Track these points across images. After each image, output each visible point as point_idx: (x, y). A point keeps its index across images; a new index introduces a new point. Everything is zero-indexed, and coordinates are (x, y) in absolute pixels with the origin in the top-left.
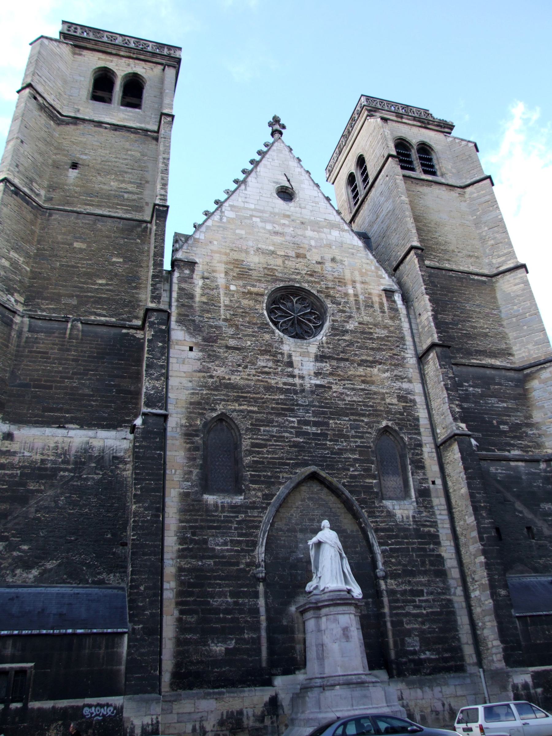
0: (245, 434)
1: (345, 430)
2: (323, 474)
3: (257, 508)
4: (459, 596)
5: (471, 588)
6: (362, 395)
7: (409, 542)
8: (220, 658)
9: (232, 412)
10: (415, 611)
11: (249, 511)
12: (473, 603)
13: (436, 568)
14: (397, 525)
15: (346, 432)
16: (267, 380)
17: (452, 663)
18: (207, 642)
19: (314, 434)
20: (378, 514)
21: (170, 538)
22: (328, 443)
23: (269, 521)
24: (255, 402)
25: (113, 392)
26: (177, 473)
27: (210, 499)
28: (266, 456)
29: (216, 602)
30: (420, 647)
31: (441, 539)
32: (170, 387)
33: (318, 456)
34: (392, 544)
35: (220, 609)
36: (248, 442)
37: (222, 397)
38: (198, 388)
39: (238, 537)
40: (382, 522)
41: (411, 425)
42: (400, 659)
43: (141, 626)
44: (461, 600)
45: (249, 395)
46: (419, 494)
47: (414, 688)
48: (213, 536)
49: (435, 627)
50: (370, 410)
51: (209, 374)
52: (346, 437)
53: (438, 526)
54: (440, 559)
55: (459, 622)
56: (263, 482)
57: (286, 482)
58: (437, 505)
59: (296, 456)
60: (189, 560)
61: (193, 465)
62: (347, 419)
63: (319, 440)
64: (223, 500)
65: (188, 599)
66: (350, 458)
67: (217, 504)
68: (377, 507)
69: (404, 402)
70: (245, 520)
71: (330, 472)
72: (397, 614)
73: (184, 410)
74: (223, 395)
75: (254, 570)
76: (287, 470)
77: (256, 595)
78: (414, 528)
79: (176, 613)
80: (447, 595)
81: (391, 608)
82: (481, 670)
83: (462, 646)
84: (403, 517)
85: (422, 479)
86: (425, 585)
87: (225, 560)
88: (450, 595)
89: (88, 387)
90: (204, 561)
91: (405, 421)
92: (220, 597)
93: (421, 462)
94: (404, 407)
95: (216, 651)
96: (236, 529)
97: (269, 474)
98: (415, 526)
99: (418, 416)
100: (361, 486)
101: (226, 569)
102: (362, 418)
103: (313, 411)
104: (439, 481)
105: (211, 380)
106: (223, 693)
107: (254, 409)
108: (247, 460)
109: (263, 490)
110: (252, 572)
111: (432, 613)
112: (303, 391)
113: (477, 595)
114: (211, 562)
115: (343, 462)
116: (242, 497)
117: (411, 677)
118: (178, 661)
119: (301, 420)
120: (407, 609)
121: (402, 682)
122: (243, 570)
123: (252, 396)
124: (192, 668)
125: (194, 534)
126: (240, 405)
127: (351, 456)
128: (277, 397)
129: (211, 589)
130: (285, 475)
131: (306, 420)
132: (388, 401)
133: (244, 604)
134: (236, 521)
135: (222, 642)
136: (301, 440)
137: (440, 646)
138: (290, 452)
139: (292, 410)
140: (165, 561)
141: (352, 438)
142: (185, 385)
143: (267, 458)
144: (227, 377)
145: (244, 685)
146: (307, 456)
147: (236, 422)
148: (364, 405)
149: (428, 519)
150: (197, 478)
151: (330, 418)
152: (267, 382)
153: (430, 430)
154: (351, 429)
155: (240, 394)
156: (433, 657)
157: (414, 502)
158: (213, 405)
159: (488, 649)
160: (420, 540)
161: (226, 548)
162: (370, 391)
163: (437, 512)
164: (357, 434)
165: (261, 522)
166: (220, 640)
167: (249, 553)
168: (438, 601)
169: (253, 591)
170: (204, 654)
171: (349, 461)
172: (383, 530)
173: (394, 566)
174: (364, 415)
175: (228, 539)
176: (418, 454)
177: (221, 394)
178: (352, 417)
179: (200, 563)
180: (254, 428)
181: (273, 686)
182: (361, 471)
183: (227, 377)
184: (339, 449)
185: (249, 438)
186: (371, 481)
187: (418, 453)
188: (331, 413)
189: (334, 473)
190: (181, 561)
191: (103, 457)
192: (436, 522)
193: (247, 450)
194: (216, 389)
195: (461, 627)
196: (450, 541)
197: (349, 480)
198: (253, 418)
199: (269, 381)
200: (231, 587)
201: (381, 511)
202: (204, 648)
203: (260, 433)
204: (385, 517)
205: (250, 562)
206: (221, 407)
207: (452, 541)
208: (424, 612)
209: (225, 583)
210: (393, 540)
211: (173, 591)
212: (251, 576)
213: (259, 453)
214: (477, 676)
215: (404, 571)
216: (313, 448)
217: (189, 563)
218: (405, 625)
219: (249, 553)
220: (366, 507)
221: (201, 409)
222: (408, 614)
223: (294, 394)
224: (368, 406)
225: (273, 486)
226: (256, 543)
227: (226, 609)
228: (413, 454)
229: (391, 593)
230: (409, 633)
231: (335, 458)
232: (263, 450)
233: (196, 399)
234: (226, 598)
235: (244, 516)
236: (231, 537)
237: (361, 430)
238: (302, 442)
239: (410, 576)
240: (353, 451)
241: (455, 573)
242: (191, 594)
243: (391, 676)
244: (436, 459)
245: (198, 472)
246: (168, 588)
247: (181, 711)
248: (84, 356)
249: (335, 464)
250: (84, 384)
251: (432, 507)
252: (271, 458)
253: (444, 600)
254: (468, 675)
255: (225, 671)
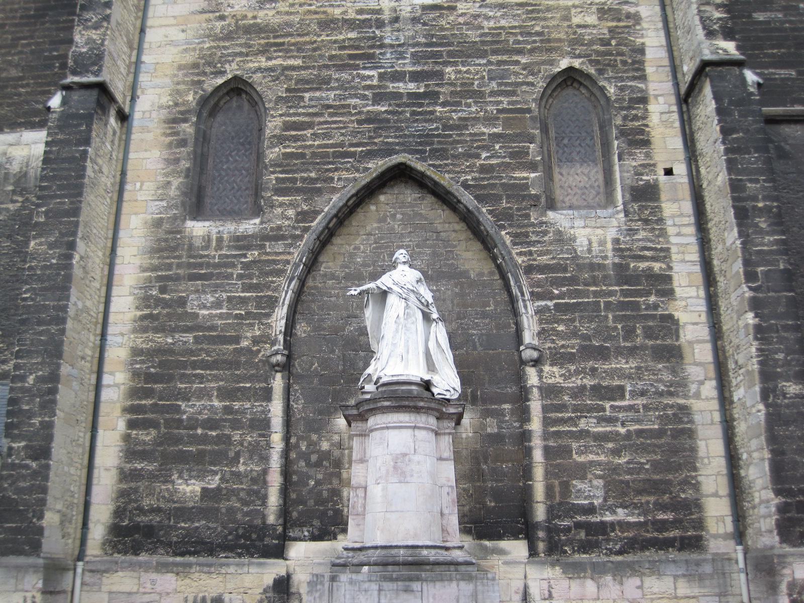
0: (273, 109)
1: (476, 83)
2: (420, 166)
3: (283, 238)
4: (707, 399)
5: (734, 382)
6: (519, 15)
7: (602, 290)
8: (191, 504)
9: (254, 73)
10: (601, 429)
11: (268, 244)
12: (737, 412)
13: (658, 342)
14: (576, 257)
15: (479, 86)
16: (325, 9)
17: (674, 533)
18: (170, 477)
19: (410, 95)
20: (534, 238)
21: (122, 299)
22: (438, 109)
23: (301, 260)
24: (299, 50)
25: (55, 67)
26: (144, 187)
27: (198, 228)
28: (310, 143)
29: (189, 409)
30: (605, 500)
31: (676, 283)
32: (146, 46)
33: (414, 136)
34: (559, 297)
35: (197, 419)
36: (278, 121)
37: (238, 50)
38: (197, 41)
39: (243, 292)
40: (541, 254)
41: (624, 63)
42: (557, 521)
43: (23, 444)
44: (711, 408)
45: (289, 39)
46: (631, 194)
47: (580, 578)
48: (197, 291)
49: (643, 460)
50: (535, 42)
51: (218, 14)
52: (478, 95)
53: (670, 258)
54: (670, 325)
55: (702, 452)
56: (298, 191)
57: (345, 187)
58: (673, 217)
59: (370, 137)
60: (150, 335)
61: (174, 171)
62: (485, 61)
63: (421, 105)
64: (221, 229)
65: (143, 402)
66: (484, 134)
67: (208, 236)
68: (533, 225)
69: (612, 20)
70: (259, 261)
71: (438, 162)
72: (558, 434)
73: (168, 81)
74: (241, 45)
75: (267, 350)
76: (349, 165)
77: (267, 395)
78: (614, 264)
79: (121, 425)
80: (678, 396)
81: (547, 422)
82: (739, 548)
83: (703, 500)
84: (590, 243)
85: (644, 166)
86: (629, 377)
87: (215, 334)
88: (686, 397)
89: (16, 66)
90: (177, 336)
91: (611, 54)
92: (199, 398)
93: (642, 132)
94: (611, 30)
95: (185, 494)
96: (240, 277)
97: (313, 175)
98: (617, 260)
99: (643, 44)
100: (503, 185)
101: (215, 350)
102: (515, 58)
103: (412, 54)
104: (681, 169)
105: (219, 24)
106: (190, 565)
107: (296, 63)
108: (273, 154)
109: (298, 205)
110: (262, 353)
111: (640, 433)
112: (396, 19)
113: (741, 396)
114: (189, 337)
115: (466, 141)
116: (257, 221)
117: (577, 556)
118: (119, 507)
119: (385, 73)
120: (583, 424)
121: (553, 565)
122: (248, 350)
123: (293, 41)
124: (143, 519)
125: (163, 290)
126: (269, 59)
127: (485, 130)
128: (341, 37)
129: (183, 386)
130: (345, 175)
131: (396, 71)
132: (576, 20)
133: (243, 412)
134: (242, 263)
135: (197, 477)
136: (383, 109)
137: (652, 499)
138: (358, 132)
139: (370, 57)
140: (109, 338)
141: (490, 96)
142: (174, 38)
143: (311, 146)
144: (250, 15)
145: (230, 554)
146: (392, 137)
147: (258, 89)
148: (521, 34)
149: (650, 245)
150: (178, 193)
151: (446, 64)
152: (325, 12)
153: (668, 69)
154: (490, 79)
155: (272, 41)
156: (631, 519)
157: (620, 211)
158: (219, 65)
159: (754, 507)
160: (625, 287)
161: (218, 311)
162: (539, 5)
163: (671, 230)
164: (503, 88)
165: (288, 262)
166: (194, 473)
167: (260, 319)
168: (657, 409)
169: (261, 388)
170: (164, 497)
171: (479, 140)
172: (542, 269)
173: (563, 339)
174: (520, 52)
175: (224, 295)
176: (636, 118)
177: (237, 45)
178: (494, 58)
179: (170, 340)
180: (293, 97)
181: (286, 559)
182: (505, 157)
183: (250, 15)
184: (460, 119)
185: (281, 115)
186: (525, 175)
187: (636, 115)
188: (451, 54)
189: (446, 165)
190: (137, 338)
191: (26, 174)
192: (668, 250)
193: (274, 136)
194: (229, 37)
195: (706, 461)
196: (698, 287)
197: (477, 175)
198: (291, 80)
199: (330, 10)
200: (222, 380)
201: (541, 232)
202: (163, 487)
203: (302, 104)
204: (551, 243)
205: (261, 336)
206: (234, 66)
207: (702, 288)
208: (622, 430)
209: (210, 375)
210: (564, 289)
211: (119, 388)
212: (260, 361)
213: (296, 139)
214: (730, 559)
215: (583, 348)
216: (407, 120)
217: (151, 341)
218: (575, 456)
219: (260, 319)
220: (511, 226)
221: (198, 74)
222: (583, 434)
223: (377, 28)
224: (530, 34)
225: (318, 196)
226: (276, 301)
227: (209, 420)
228: (625, 118)
229: (548, 391)
230: (582, 471)
231: (451, 136)
232: (305, 132)
233: (189, 58)
234: (212, 401)
235: (256, 253)
236: (231, 291)
237: (513, 79)
238: (386, 111)
239: (596, 359)
240: (490, 120)
241: (703, 353)
242: (148, 393)
243: (533, 552)
244: (677, 124)
245: (181, 183)
246: (112, 383)
247: (115, 588)
248: (14, 18)
249: (449, 147)
250: (10, 63)
251: (661, 220)
252: (319, 146)
253: (672, 406)
254: (709, 557)
255: (197, 528)
